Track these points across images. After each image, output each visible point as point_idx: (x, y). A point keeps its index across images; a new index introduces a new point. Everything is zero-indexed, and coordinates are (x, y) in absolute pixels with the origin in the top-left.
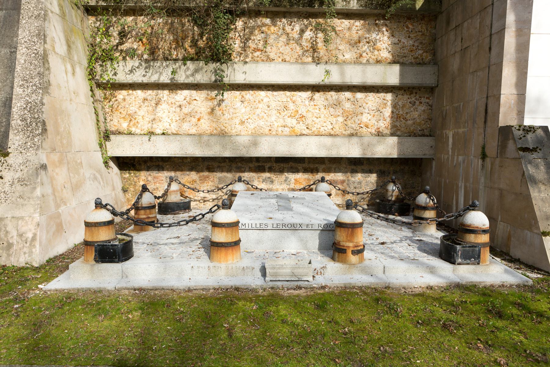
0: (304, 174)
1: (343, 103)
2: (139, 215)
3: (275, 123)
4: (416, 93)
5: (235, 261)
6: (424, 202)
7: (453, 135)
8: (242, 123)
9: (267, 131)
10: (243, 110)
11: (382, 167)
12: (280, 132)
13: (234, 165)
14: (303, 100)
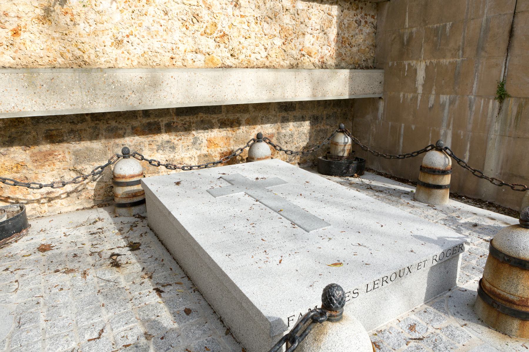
1: (280, 15)
3: (180, 45)
4: (362, 8)
6: (442, 163)
7: (427, 67)
8: (119, 43)
9: (166, 60)
10: (117, 17)
11: (315, 112)
12: (191, 62)
13: (103, 126)
14: (224, 6)
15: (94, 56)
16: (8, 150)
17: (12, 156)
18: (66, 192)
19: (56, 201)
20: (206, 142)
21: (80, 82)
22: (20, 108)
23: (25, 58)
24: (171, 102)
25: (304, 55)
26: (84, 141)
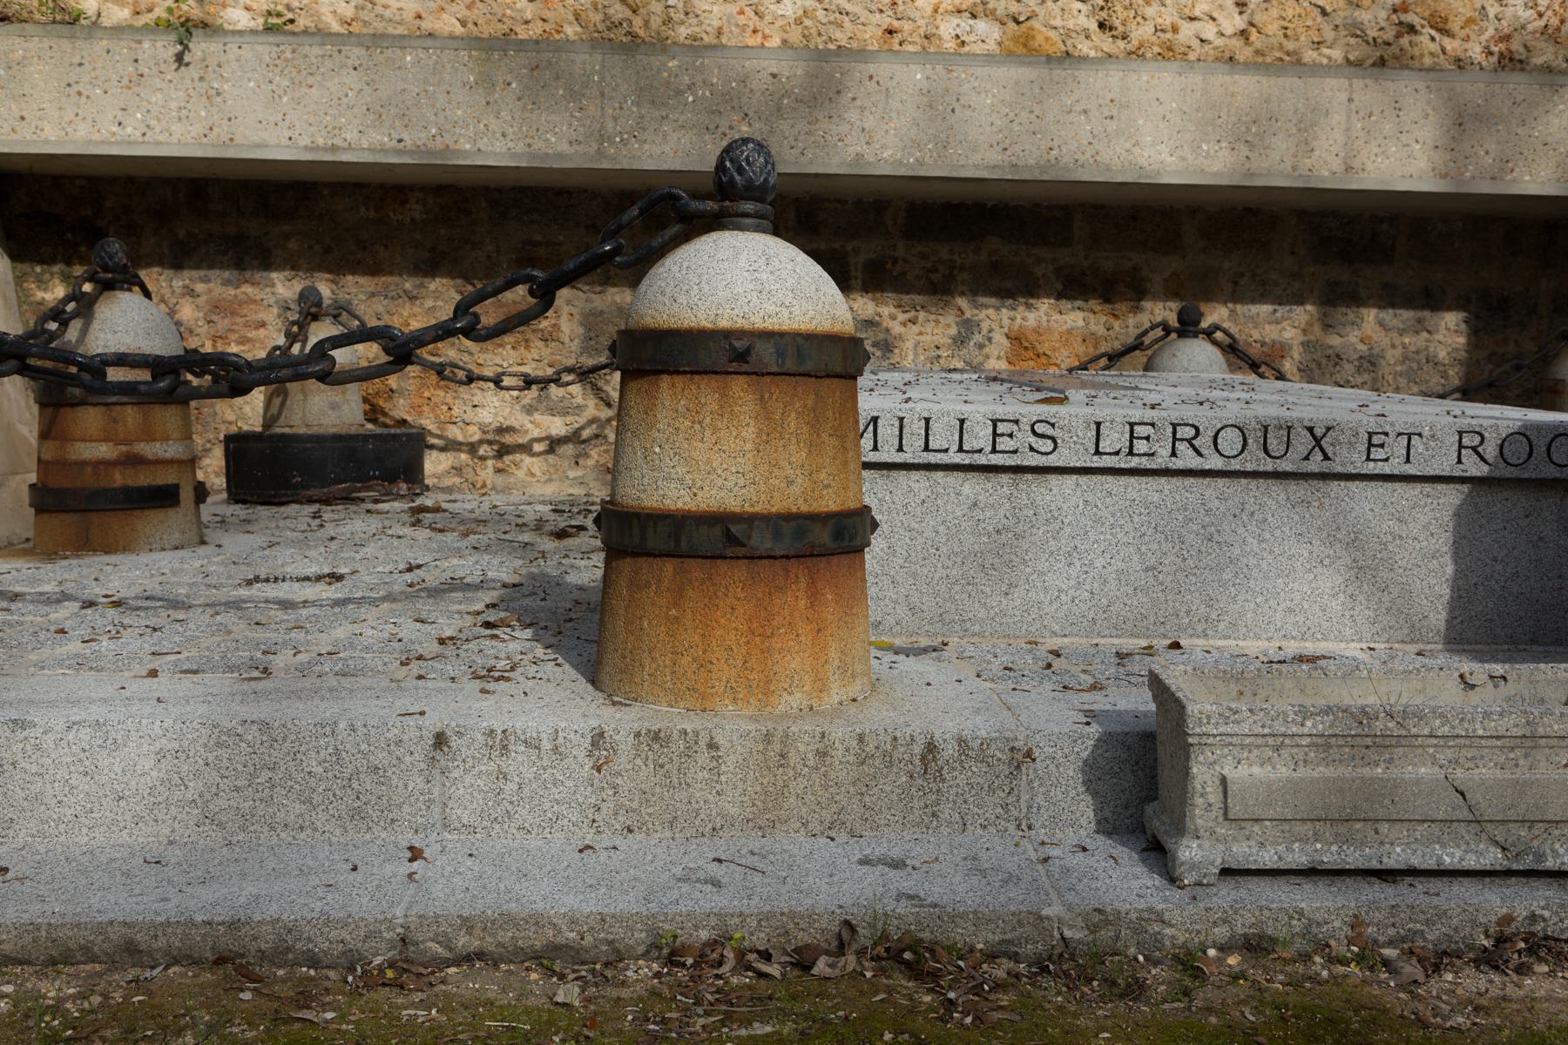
0: (1066, 304)
2: (65, 439)
5: (837, 693)
9: (871, 36)
15: (659, 21)
16: (422, 285)
17: (429, 303)
18: (547, 438)
19: (518, 457)
20: (1005, 341)
21: (602, 79)
22: (448, 139)
23: (488, 22)
25: (1412, 29)
26: (615, 285)
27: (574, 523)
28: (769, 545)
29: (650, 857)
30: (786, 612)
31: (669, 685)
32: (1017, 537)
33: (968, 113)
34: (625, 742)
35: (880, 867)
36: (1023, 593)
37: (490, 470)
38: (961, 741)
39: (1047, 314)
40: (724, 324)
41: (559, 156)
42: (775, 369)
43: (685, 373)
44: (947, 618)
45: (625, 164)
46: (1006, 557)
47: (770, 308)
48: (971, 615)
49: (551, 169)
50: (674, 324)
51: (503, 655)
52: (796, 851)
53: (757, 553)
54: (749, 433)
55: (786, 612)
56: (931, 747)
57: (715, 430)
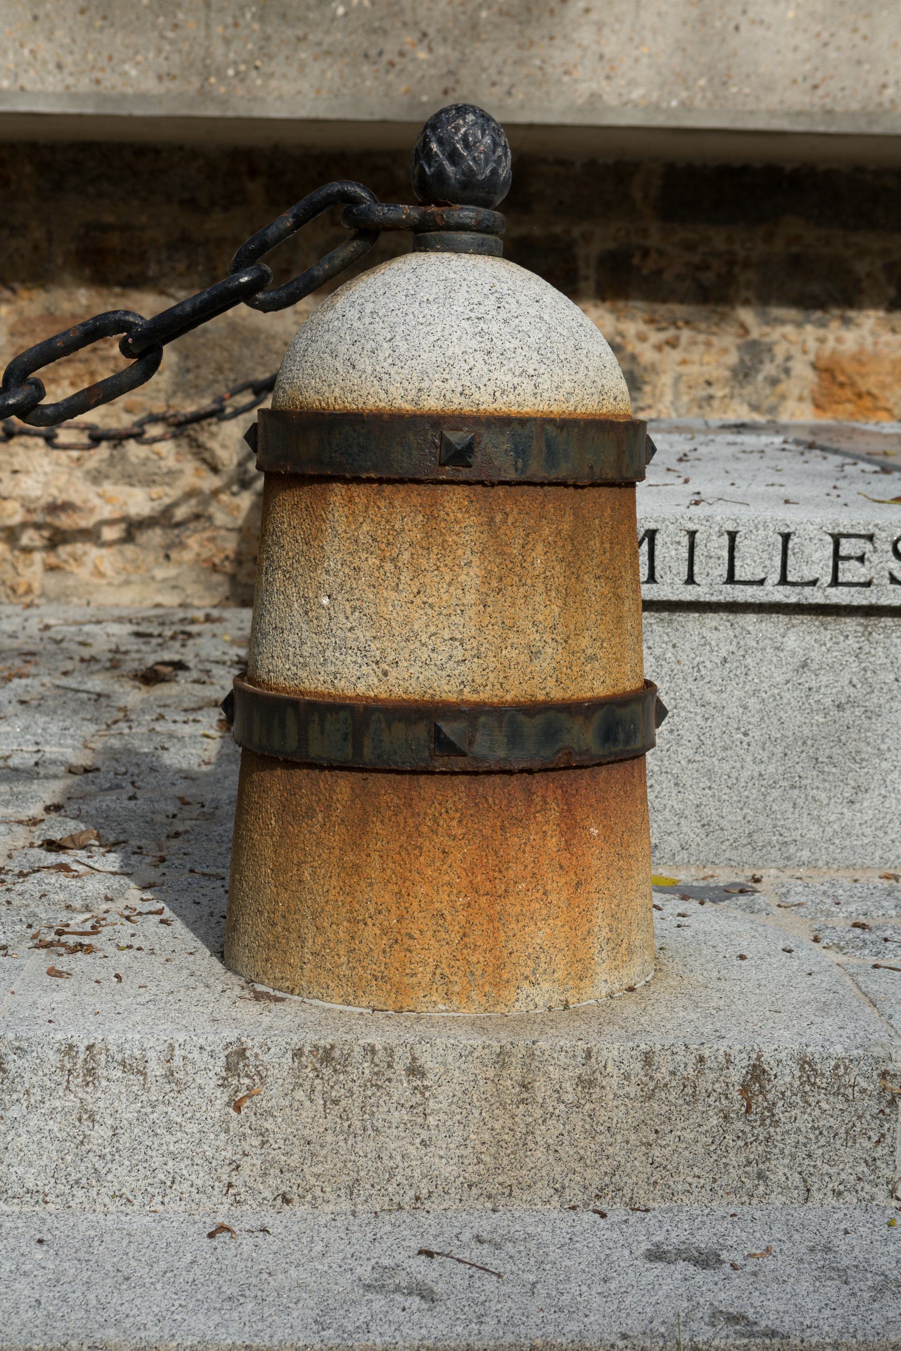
5: (605, 980)
20: (810, 375)
24: (595, 97)
27: (167, 656)
28: (501, 753)
29: (319, 1247)
30: (528, 858)
31: (344, 970)
32: (869, 714)
33: (760, 32)
34: (278, 1065)
35: (681, 1264)
36: (877, 801)
37: (38, 568)
38: (805, 1063)
39: (873, 333)
40: (432, 404)
41: (143, 97)
42: (511, 475)
43: (370, 481)
44: (760, 839)
45: (241, 108)
46: (851, 746)
47: (504, 378)
48: (796, 835)
49: (130, 119)
50: (351, 402)
51: (77, 904)
52: (546, 1236)
53: (484, 766)
54: (472, 576)
55: (528, 858)
56: (757, 1073)
57: (418, 572)
